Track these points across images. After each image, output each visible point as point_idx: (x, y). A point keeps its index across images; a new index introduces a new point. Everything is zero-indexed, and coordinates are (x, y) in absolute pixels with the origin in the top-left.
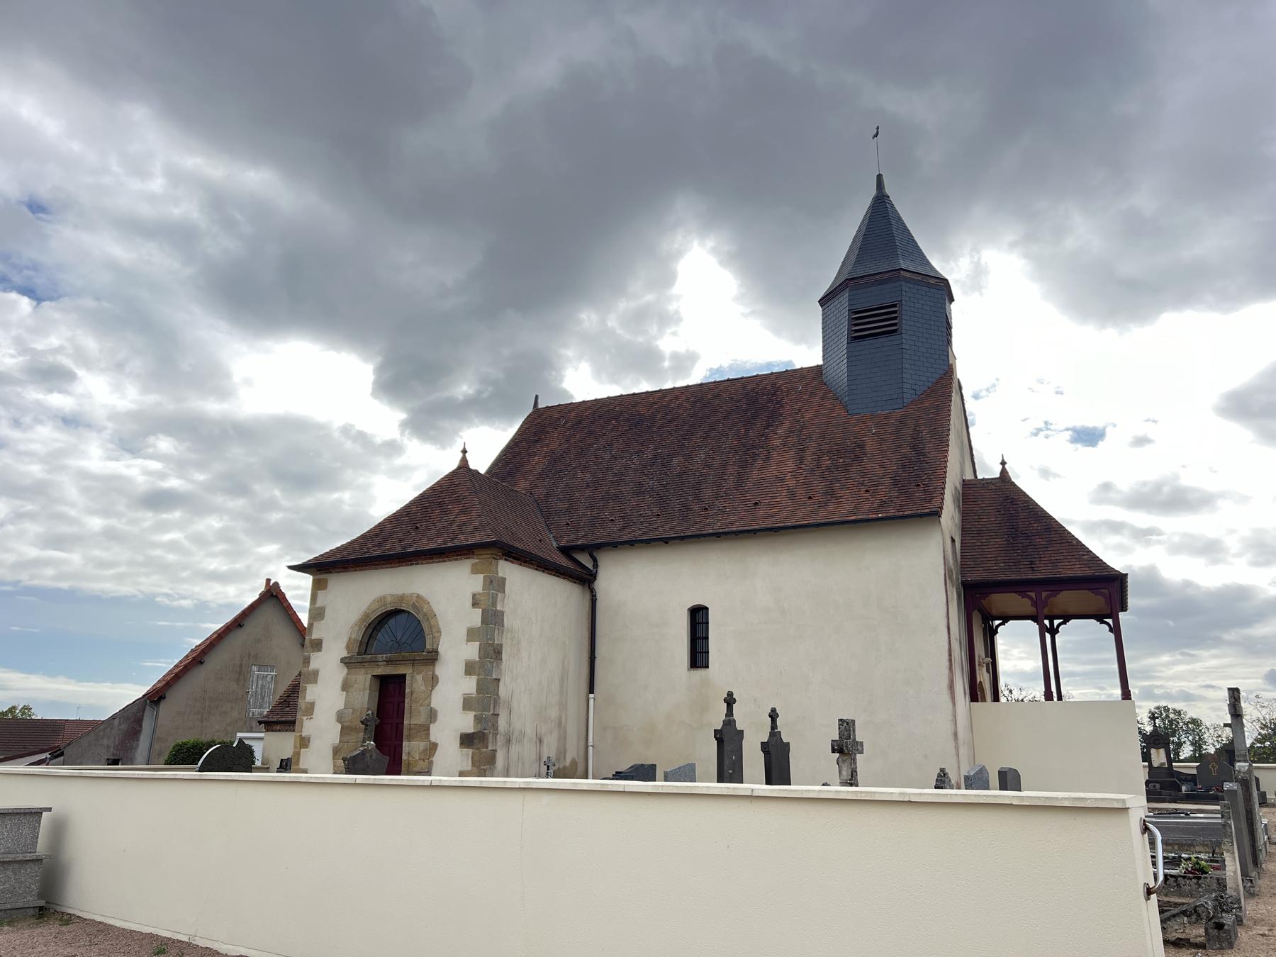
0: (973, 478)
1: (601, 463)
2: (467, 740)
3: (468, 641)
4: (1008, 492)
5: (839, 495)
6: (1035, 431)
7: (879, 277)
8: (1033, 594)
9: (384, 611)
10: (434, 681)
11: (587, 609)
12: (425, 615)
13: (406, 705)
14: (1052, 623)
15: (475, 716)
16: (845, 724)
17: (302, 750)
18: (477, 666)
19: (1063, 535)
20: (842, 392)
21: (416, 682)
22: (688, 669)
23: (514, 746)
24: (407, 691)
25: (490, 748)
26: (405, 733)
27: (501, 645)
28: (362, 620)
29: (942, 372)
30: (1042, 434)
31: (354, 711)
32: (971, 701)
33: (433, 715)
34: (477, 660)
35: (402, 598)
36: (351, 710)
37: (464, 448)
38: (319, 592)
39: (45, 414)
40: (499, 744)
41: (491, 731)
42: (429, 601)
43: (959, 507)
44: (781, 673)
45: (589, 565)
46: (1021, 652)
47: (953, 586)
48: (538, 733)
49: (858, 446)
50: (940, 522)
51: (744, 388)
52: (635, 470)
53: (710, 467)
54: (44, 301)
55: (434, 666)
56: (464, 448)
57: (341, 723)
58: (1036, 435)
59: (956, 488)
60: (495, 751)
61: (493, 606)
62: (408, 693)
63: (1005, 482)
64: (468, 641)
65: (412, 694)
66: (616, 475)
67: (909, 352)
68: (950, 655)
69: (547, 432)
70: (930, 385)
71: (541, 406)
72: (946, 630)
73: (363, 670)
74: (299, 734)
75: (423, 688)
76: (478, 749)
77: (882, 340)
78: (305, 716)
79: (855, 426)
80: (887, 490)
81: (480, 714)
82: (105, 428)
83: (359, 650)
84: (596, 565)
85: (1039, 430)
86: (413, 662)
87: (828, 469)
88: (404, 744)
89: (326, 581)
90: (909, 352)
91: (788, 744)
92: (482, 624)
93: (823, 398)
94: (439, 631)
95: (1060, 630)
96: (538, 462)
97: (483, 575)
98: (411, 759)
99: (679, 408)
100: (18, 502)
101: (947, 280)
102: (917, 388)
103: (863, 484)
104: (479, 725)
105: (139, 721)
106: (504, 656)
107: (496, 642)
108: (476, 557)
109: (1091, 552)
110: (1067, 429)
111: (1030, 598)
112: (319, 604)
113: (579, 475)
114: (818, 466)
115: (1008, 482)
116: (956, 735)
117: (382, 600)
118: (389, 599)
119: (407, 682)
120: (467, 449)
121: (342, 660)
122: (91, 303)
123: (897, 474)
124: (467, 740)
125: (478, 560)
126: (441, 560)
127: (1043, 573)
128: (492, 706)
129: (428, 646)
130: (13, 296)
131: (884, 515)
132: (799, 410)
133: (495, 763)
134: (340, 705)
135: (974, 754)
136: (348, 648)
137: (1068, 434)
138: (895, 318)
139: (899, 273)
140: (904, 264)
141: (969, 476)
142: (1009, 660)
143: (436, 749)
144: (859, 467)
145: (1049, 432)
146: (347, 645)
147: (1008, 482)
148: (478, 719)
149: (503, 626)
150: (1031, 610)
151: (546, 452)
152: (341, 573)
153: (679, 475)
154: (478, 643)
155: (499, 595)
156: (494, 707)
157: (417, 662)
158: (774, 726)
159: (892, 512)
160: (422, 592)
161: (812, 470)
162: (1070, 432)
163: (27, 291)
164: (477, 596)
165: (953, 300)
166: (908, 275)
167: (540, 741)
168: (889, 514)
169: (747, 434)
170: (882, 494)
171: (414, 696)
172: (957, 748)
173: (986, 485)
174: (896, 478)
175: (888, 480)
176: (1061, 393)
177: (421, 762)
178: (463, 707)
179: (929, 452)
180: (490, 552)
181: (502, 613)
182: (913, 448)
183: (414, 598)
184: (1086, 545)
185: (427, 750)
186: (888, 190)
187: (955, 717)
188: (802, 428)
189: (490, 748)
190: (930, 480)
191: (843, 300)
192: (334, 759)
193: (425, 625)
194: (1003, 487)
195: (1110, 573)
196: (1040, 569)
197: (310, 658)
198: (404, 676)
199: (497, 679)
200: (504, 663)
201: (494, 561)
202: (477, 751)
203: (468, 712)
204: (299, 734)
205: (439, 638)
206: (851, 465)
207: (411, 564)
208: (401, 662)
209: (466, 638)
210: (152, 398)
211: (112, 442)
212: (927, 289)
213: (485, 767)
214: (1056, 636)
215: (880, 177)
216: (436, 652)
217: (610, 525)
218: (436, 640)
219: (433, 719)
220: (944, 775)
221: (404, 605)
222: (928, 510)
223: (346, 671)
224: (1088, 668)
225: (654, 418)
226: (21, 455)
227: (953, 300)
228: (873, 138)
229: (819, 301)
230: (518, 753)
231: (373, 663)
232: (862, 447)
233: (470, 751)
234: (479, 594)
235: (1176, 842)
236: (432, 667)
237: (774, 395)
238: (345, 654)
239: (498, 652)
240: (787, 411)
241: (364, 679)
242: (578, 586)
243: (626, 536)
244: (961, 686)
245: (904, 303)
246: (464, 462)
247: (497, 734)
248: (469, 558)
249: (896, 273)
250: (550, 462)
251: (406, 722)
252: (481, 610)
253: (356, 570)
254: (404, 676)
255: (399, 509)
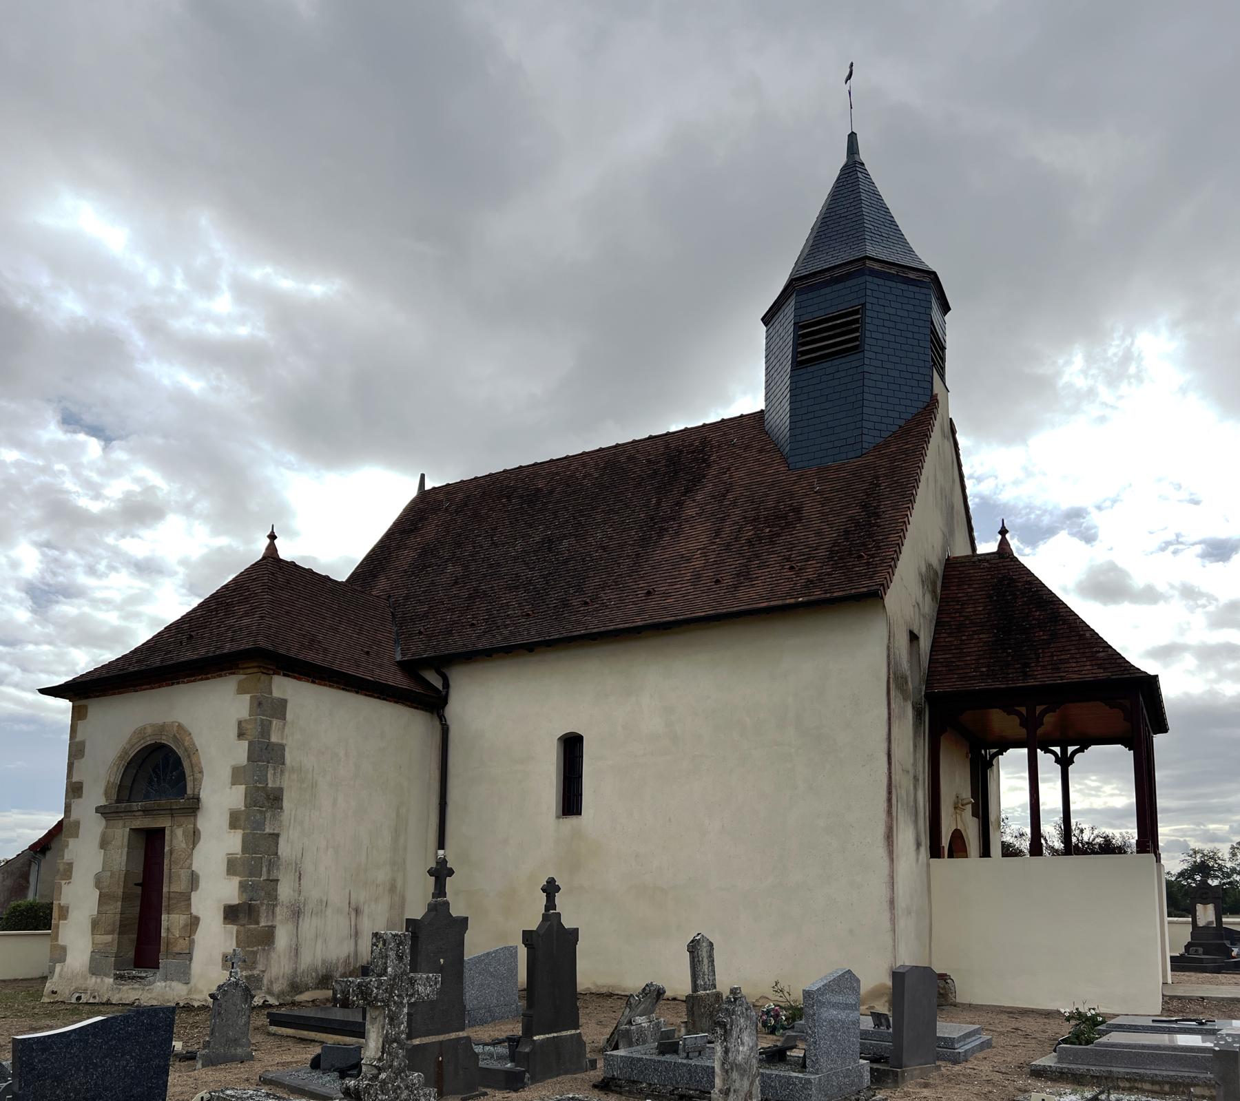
0: (969, 552)
1: (478, 552)
2: (231, 914)
3: (233, 784)
4: (1006, 571)
5: (755, 576)
6: (1163, 545)
7: (837, 273)
8: (1023, 710)
9: (144, 746)
10: (195, 836)
11: (438, 743)
12: (186, 750)
13: (165, 867)
14: (1064, 751)
15: (240, 882)
16: (380, 945)
17: (61, 922)
18: (243, 817)
19: (1073, 625)
20: (784, 440)
21: (176, 839)
22: (558, 817)
23: (307, 920)
24: (167, 849)
25: (262, 924)
26: (164, 904)
27: (281, 790)
28: (121, 758)
29: (921, 405)
30: (1171, 548)
31: (113, 874)
32: (932, 857)
33: (194, 881)
34: (243, 808)
35: (162, 728)
36: (109, 874)
37: (273, 532)
38: (79, 722)
39: (121, 560)
40: (279, 918)
41: (265, 902)
42: (191, 730)
43: (934, 592)
44: (670, 820)
45: (438, 684)
46: (1113, 789)
47: (905, 699)
48: (353, 902)
49: (793, 510)
50: (884, 606)
51: (667, 447)
52: (515, 558)
53: (604, 549)
54: (114, 440)
55: (195, 816)
56: (273, 532)
57: (98, 889)
58: (1163, 549)
59: (929, 566)
60: (273, 927)
61: (263, 737)
62: (167, 852)
63: (1003, 558)
64: (233, 784)
65: (171, 854)
66: (491, 566)
67: (874, 377)
68: (890, 793)
69: (426, 519)
70: (902, 423)
71: (428, 486)
72: (885, 759)
73: (121, 823)
74: (58, 902)
75: (184, 845)
76: (244, 925)
77: (836, 362)
78: (64, 880)
79: (795, 483)
80: (819, 565)
81: (245, 881)
82: (176, 573)
83: (118, 796)
84: (446, 685)
85: (1168, 544)
86: (172, 813)
87: (749, 541)
88: (163, 916)
89: (85, 707)
90: (874, 377)
91: (575, 932)
92: (248, 761)
93: (760, 451)
94: (201, 772)
95: (1075, 759)
96: (407, 556)
97: (249, 695)
98: (170, 936)
99: (585, 477)
100: (96, 651)
101: (934, 273)
102: (883, 427)
103: (788, 560)
104: (244, 894)
105: (25, 877)
106: (286, 804)
107: (270, 785)
108: (241, 671)
109: (1110, 647)
110: (1200, 543)
111: (1019, 714)
112: (78, 739)
113: (450, 569)
114: (737, 539)
115: (1008, 557)
116: (892, 902)
117: (140, 732)
118: (149, 731)
119: (167, 838)
120: (276, 534)
121: (98, 810)
122: (160, 441)
123: (835, 544)
124: (231, 914)
125: (245, 676)
126: (204, 677)
127: (1041, 677)
128: (264, 869)
129: (189, 791)
130: (81, 437)
131: (806, 599)
132: (729, 469)
133: (273, 942)
134: (98, 868)
135: (931, 924)
136: (106, 794)
137: (1199, 549)
138: (856, 330)
139: (864, 264)
140: (872, 250)
141: (961, 550)
142: (1099, 796)
143: (198, 924)
144: (788, 537)
145: (1180, 547)
146: (106, 790)
147: (1008, 557)
148: (243, 887)
149: (283, 763)
150: (1022, 733)
151: (419, 544)
152: (100, 698)
153: (566, 562)
154: (244, 786)
155: (275, 722)
156: (269, 872)
157: (177, 811)
158: (551, 904)
159: (818, 594)
160: (184, 720)
161: (729, 545)
162: (1203, 546)
163: (95, 431)
164: (243, 725)
165: (949, 309)
166: (877, 266)
167: (357, 911)
168: (812, 598)
169: (658, 503)
170: (810, 573)
171: (174, 855)
172: (893, 920)
173: (977, 563)
174: (833, 549)
175: (822, 553)
176: (1197, 503)
177: (181, 941)
178: (227, 871)
179: (883, 512)
180: (255, 664)
181: (282, 747)
182: (865, 507)
183: (175, 729)
184: (1105, 639)
185: (187, 926)
186: (863, 156)
187: (892, 878)
188: (728, 491)
189: (262, 924)
190: (879, 548)
191: (789, 311)
192: (92, 934)
193: (186, 764)
194: (1000, 565)
195: (1132, 676)
196: (1036, 673)
197: (71, 804)
198: (163, 830)
199: (273, 834)
200: (285, 812)
201: (263, 677)
202: (242, 928)
203: (232, 877)
204: (58, 902)
205: (202, 779)
206: (779, 535)
207: (173, 684)
208: (158, 812)
209: (230, 780)
210: (224, 541)
211: (183, 586)
212: (904, 287)
213: (255, 949)
214: (1070, 768)
215: (852, 137)
216: (197, 799)
217: (469, 630)
218: (197, 782)
219: (194, 885)
220: (736, 999)
221: (164, 737)
222: (865, 590)
223: (104, 822)
224: (1184, 803)
225: (551, 492)
226: (94, 602)
227: (949, 309)
228: (846, 83)
229: (762, 319)
230: (317, 927)
231: (130, 814)
232: (797, 510)
233: (233, 928)
234: (246, 720)
235: (1168, 1079)
236: (192, 818)
237: (702, 451)
238: (102, 802)
239: (274, 800)
240: (713, 472)
241: (121, 833)
242: (422, 712)
243: (483, 644)
244: (908, 836)
245: (868, 306)
246: (272, 549)
247: (275, 906)
248: (234, 673)
249: (860, 263)
250: (420, 555)
251: (165, 890)
252: (247, 743)
253: (114, 694)
254: (163, 830)
255: (185, 613)
